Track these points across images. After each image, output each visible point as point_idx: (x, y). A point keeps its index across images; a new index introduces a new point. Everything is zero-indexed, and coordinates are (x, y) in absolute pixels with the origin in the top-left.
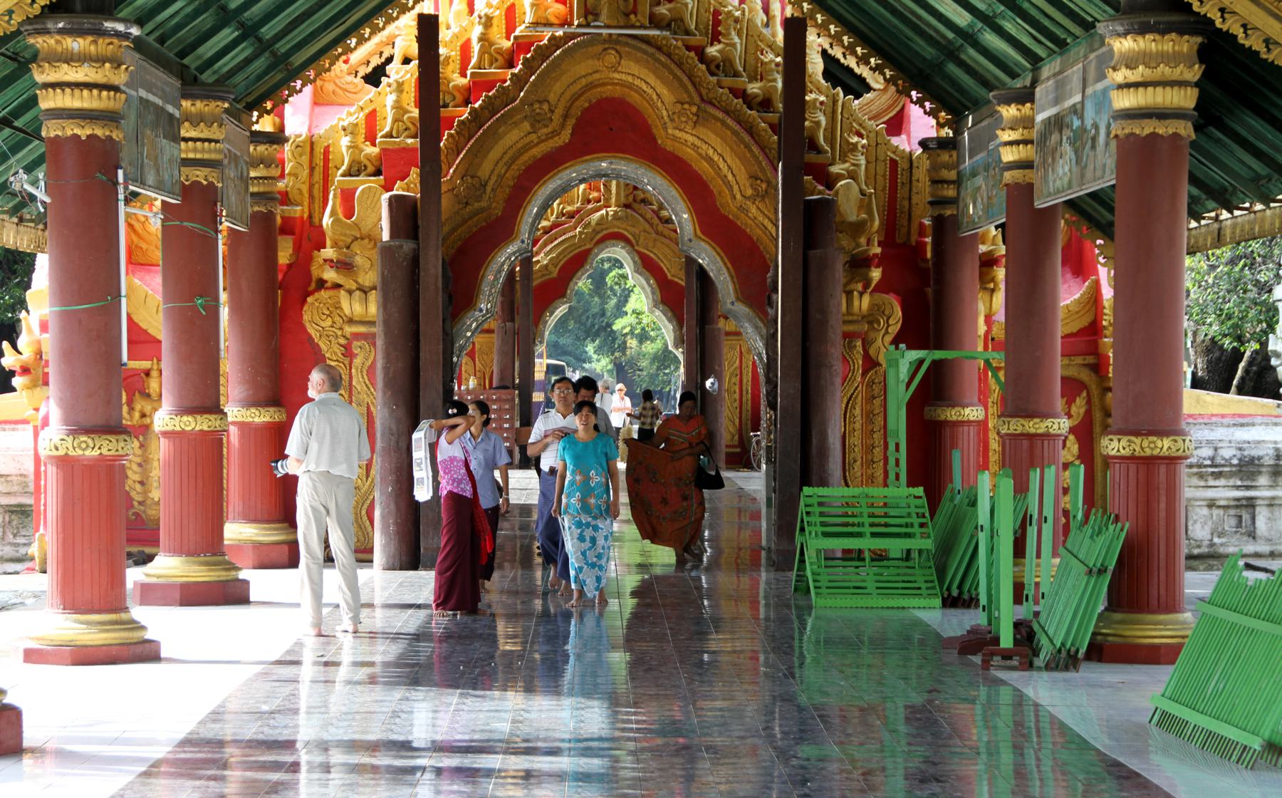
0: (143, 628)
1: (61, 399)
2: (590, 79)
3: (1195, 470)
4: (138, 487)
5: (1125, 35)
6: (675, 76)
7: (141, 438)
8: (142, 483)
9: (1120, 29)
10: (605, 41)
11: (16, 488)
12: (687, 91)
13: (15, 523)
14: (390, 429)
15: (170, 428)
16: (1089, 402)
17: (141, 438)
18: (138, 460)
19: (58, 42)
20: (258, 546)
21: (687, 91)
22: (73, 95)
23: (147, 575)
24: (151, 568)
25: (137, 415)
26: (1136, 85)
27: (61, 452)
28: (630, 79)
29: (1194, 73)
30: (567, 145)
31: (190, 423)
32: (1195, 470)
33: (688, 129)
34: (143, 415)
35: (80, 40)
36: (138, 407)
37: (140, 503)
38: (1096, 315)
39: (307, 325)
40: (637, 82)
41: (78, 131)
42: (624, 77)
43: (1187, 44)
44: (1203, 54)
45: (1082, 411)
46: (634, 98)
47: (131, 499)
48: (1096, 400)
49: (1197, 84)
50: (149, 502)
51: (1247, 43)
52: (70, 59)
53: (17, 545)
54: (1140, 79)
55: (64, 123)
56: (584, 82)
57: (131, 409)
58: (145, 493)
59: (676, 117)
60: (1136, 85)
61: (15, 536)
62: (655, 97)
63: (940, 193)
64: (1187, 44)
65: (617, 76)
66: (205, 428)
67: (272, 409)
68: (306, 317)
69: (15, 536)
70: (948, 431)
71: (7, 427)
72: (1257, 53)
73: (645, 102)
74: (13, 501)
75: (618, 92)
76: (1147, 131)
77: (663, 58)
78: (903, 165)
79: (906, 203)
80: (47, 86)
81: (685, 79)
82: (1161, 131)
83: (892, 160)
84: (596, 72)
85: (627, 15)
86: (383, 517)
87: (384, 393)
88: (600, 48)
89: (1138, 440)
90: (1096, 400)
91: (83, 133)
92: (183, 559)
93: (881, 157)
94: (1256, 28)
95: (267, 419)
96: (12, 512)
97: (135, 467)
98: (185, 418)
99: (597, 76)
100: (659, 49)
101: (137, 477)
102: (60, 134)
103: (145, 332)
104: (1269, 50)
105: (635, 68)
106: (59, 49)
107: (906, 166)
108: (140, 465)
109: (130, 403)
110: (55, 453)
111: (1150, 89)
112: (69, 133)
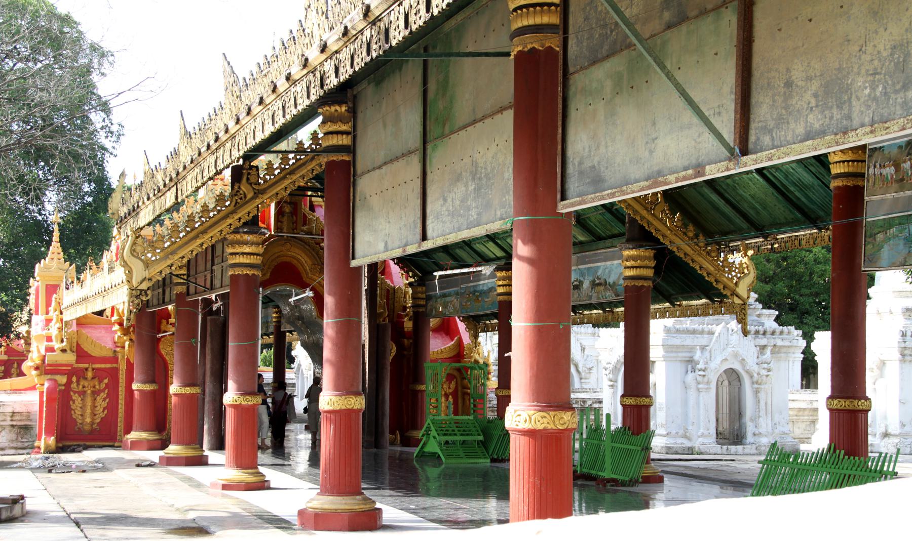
0: (264, 476)
1: (237, 381)
2: (279, 254)
3: (491, 409)
4: (80, 417)
5: (632, 249)
6: (312, 254)
7: (82, 397)
8: (82, 415)
9: (631, 246)
10: (285, 240)
11: (24, 418)
12: (316, 260)
13: (22, 433)
14: (213, 393)
15: (180, 392)
16: (457, 383)
17: (82, 397)
18: (80, 406)
19: (241, 237)
20: (148, 441)
21: (316, 260)
22: (247, 258)
23: (166, 453)
24: (166, 450)
25: (81, 387)
26: (636, 267)
27: (238, 403)
28: (295, 254)
29: (653, 264)
30: (268, 280)
31: (188, 390)
32: (491, 409)
33: (317, 275)
34: (84, 387)
35: (251, 236)
36: (82, 383)
37: (80, 424)
38: (460, 349)
39: (161, 350)
40: (297, 256)
41: (248, 272)
42: (292, 254)
43: (650, 253)
44: (656, 257)
45: (454, 386)
46: (295, 262)
47: (77, 422)
48: (459, 382)
49: (654, 268)
50: (85, 423)
51: (678, 254)
52: (246, 243)
53: (23, 442)
54: (638, 265)
55: (242, 269)
56: (277, 255)
57: (78, 384)
58: (83, 419)
59: (312, 270)
60: (636, 267)
61: (22, 438)
62: (304, 262)
63: (418, 303)
64: (650, 253)
65: (289, 253)
66: (194, 392)
67: (154, 384)
68: (161, 347)
69: (22, 438)
70: (420, 395)
71: (17, 392)
72: (681, 258)
73: (299, 265)
74: (23, 423)
75: (288, 259)
76: (641, 284)
77: (307, 247)
78: (391, 291)
79: (392, 306)
80: (232, 254)
81: (315, 255)
82: (645, 285)
83: (387, 289)
84: (281, 251)
85: (293, 230)
86: (209, 429)
87: (211, 378)
88: (284, 242)
89: (639, 399)
90: (459, 382)
91: (250, 272)
92: (184, 446)
93: (384, 288)
94: (681, 249)
95: (152, 388)
96: (21, 428)
97: (79, 409)
98: (187, 388)
99: (282, 253)
100: (305, 243)
101: (80, 413)
102: (241, 273)
103: (86, 352)
104: (685, 258)
105: (297, 251)
106: (241, 239)
107: (392, 292)
108: (81, 408)
109: (78, 382)
110: (235, 403)
111: (642, 269)
112: (245, 273)
